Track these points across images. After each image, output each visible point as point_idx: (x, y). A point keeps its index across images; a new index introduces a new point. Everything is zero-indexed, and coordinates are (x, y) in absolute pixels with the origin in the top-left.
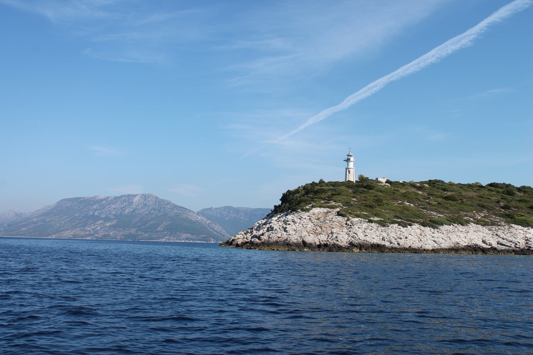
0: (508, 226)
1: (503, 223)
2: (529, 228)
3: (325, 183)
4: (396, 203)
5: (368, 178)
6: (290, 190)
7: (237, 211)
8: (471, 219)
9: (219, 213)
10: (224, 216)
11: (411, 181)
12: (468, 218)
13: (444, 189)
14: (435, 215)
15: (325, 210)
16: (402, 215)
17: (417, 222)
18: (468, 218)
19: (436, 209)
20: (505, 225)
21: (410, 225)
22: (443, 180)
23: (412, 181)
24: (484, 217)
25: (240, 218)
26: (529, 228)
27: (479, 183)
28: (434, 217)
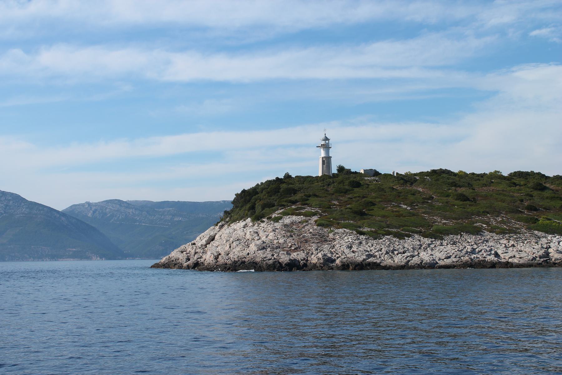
0: (530, 233)
1: (523, 230)
2: (555, 235)
3: (292, 177)
4: (389, 207)
5: (350, 169)
6: (245, 189)
7: (128, 205)
8: (483, 225)
9: (99, 212)
10: (108, 215)
11: (408, 171)
12: (480, 224)
13: (452, 183)
14: (440, 222)
15: (301, 218)
16: (208, 350)
17: (417, 232)
18: (480, 224)
19: (440, 213)
20: (526, 233)
21: (409, 236)
22: (450, 170)
23: (409, 172)
24: (502, 222)
25: (135, 218)
26: (555, 235)
27: (499, 172)
28: (437, 225)
